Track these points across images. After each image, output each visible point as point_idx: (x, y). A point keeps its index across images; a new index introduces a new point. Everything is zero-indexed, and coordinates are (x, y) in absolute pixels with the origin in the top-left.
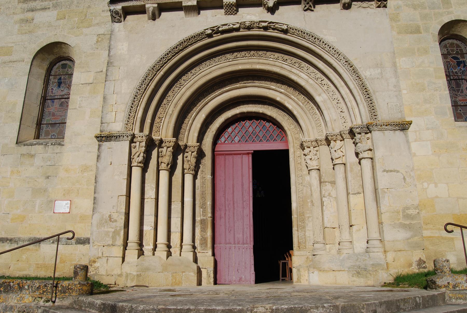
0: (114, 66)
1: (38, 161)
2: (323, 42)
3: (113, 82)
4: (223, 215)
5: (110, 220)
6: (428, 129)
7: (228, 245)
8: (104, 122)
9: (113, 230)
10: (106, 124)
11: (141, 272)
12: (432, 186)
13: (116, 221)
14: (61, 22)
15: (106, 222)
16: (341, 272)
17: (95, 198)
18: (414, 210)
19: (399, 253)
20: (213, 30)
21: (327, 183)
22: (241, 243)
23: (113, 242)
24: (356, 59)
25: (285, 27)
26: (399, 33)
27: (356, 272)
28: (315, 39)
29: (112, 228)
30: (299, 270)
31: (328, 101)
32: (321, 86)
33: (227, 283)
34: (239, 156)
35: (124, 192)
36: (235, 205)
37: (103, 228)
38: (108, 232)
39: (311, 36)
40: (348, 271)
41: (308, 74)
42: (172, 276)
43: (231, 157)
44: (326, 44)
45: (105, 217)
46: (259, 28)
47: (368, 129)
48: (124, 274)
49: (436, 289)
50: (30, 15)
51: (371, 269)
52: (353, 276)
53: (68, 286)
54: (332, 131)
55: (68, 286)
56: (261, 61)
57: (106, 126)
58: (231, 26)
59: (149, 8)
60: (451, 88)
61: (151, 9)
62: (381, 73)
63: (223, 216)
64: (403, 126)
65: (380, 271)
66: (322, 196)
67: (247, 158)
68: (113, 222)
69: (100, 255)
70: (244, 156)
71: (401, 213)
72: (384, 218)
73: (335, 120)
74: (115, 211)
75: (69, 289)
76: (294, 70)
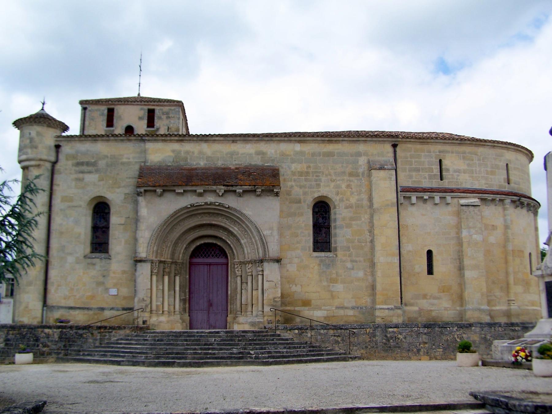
1: (98, 267)
6: (296, 258)
12: (294, 286)
14: (101, 183)
25: (227, 206)
28: (242, 214)
35: (149, 287)
50: (81, 176)
56: (215, 219)
60: (314, 232)
61: (159, 193)
64: (278, 261)
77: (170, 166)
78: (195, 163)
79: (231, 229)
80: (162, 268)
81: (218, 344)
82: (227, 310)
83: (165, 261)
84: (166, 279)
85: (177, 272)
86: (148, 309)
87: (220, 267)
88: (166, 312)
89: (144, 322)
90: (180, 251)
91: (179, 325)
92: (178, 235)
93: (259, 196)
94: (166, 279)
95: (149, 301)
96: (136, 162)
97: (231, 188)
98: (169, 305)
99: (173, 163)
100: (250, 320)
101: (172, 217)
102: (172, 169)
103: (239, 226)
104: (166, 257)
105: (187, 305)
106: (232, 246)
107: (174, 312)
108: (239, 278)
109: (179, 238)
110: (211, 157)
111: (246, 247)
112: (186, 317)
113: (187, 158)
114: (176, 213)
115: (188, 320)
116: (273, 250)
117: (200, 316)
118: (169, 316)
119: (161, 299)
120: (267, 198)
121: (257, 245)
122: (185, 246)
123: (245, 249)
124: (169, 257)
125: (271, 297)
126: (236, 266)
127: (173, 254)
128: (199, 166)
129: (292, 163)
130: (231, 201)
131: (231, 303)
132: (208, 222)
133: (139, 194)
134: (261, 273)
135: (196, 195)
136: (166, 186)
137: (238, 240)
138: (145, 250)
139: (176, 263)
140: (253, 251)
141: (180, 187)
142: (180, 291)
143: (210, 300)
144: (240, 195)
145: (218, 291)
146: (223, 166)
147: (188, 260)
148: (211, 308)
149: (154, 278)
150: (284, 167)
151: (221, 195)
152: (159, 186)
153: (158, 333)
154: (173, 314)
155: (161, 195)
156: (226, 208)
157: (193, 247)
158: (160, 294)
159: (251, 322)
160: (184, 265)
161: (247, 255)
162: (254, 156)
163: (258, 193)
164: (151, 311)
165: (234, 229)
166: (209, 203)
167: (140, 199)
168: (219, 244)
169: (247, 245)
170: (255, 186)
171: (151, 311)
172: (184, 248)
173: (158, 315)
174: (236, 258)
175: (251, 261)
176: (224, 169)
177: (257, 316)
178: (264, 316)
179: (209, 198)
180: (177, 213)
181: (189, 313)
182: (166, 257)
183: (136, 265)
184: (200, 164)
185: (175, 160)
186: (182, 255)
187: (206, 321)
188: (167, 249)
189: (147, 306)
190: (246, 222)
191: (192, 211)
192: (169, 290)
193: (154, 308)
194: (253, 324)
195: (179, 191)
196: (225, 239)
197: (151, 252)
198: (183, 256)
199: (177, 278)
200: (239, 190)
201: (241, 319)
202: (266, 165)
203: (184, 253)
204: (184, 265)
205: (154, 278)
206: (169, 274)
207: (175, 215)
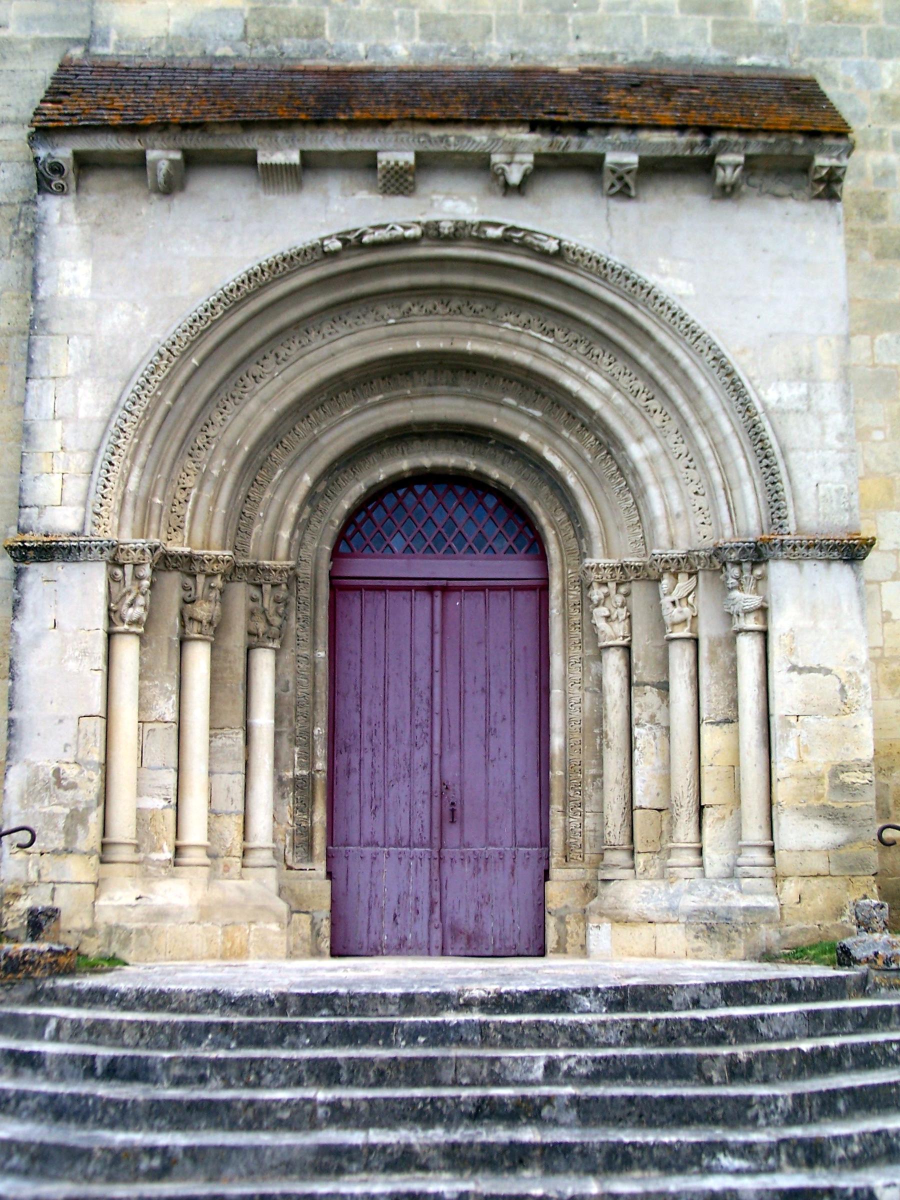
0: (50, 333)
2: (656, 298)
3: (51, 383)
4: (355, 765)
5: (58, 783)
7: (369, 849)
8: (27, 501)
9: (67, 811)
10: (35, 510)
11: (146, 924)
13: (73, 786)
15: (48, 789)
16: (668, 925)
17: (11, 723)
18: (861, 775)
19: (815, 881)
20: (345, 242)
21: (648, 688)
22: (405, 843)
23: (66, 842)
24: (743, 351)
25: (553, 246)
26: (880, 255)
27: (704, 927)
28: (637, 289)
29: (65, 806)
30: (562, 920)
31: (662, 461)
32: (647, 415)
33: (364, 951)
34: (404, 593)
35: (98, 707)
36: (392, 737)
37: (37, 806)
38: (53, 816)
39: (622, 278)
40: (687, 925)
41: (611, 379)
42: (225, 933)
43: (379, 596)
44: (662, 304)
45: (41, 775)
46: (479, 239)
47: (757, 554)
48: (102, 928)
49: (849, 965)
51: (741, 919)
52: (697, 937)
53: (24, 956)
54: (668, 546)
55: (24, 956)
56: (479, 328)
57: (35, 516)
58: (399, 231)
59: (155, 162)
61: (164, 166)
62: (808, 397)
63: (357, 767)
64: (852, 551)
65: (762, 926)
66: (634, 722)
67: (428, 600)
68: (66, 788)
69: (33, 876)
70: (418, 593)
71: (826, 781)
72: (781, 792)
73: (678, 516)
74: (72, 760)
75: (25, 963)
76: (572, 364)
77: (224, 58)
78: (361, 48)
79: (569, 383)
80: (172, 592)
81: (588, 1111)
82: (545, 842)
83: (190, 559)
84: (199, 657)
85: (261, 627)
86: (89, 838)
87: (499, 603)
88: (194, 856)
89: (39, 922)
90: (283, 508)
91: (274, 927)
92: (267, 417)
93: (727, 192)
94: (199, 657)
95: (90, 790)
96: (40, 44)
97: (572, 143)
98: (214, 813)
99: (244, 48)
100: (689, 902)
101: (238, 304)
102: (235, 71)
103: (619, 366)
104: (201, 534)
105: (320, 815)
106: (571, 480)
107: (245, 852)
108: (614, 661)
109: (274, 437)
110: (445, 18)
111: (660, 482)
112: (314, 881)
113: (319, 23)
114: (258, 280)
115: (328, 893)
116: (819, 496)
117: (393, 878)
118: (212, 877)
119: (170, 778)
120: (776, 208)
122: (308, 479)
123: (653, 492)
124: (217, 533)
125: (820, 760)
126: (597, 593)
127: (240, 521)
128: (387, 62)
129: (880, 55)
130: (568, 218)
131: (566, 800)
132: (441, 345)
133: (47, 179)
134: (751, 623)
135: (371, 189)
136: (200, 126)
137: (608, 444)
138: (76, 488)
139: (255, 574)
140: (701, 501)
141: (281, 135)
142: (277, 735)
143: (445, 787)
144: (623, 188)
145: (489, 732)
146: (511, 64)
147: (325, 565)
148: (452, 833)
149: (128, 651)
150: (840, 74)
151: (515, 176)
152: (163, 127)
153: (120, 1000)
154: (236, 862)
155: (170, 188)
157: (355, 489)
158: (162, 748)
159: (698, 912)
160: (305, 593)
161: (661, 527)
162: (677, 14)
163: (726, 176)
164: (105, 850)
165: (587, 383)
167: (53, 207)
168: (495, 474)
169: (666, 473)
170: (707, 131)
171: (105, 850)
173: (144, 870)
174: (598, 545)
175: (686, 558)
176: (524, 72)
177: (732, 875)
178: (778, 878)
179: (449, 205)
180: (262, 287)
181: (330, 857)
182: (199, 533)
183: (19, 573)
184: (388, 53)
185: (253, 30)
186: (287, 529)
187: (424, 906)
188: (207, 494)
189: (77, 818)
190: (662, 337)
191: (351, 277)
192: (215, 727)
193: (123, 827)
194: (714, 927)
195: (279, 158)
196: (536, 444)
197: (114, 505)
198: (297, 544)
199: (264, 661)
200: (621, 155)
201: (633, 892)
202: (744, 61)
203: (301, 525)
204: (305, 593)
205: (128, 651)
206: (216, 632)
207: (250, 296)
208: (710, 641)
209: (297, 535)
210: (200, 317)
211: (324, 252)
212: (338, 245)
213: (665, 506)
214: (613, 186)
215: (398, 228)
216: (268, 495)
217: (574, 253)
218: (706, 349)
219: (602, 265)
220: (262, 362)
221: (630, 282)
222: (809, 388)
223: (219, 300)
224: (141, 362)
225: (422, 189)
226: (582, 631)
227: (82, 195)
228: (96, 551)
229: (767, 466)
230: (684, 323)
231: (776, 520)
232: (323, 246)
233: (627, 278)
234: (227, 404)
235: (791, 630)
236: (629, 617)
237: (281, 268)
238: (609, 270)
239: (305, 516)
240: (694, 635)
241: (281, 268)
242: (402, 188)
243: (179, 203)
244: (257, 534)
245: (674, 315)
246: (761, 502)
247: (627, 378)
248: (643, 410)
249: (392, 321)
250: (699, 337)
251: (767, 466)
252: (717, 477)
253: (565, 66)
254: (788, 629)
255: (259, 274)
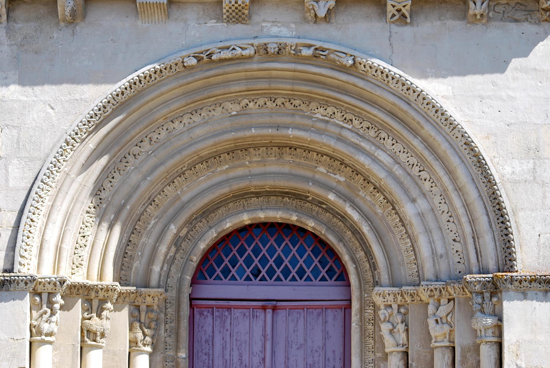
58: (239, 51)
73: (441, 256)
121: (472, 222)
140: (458, 246)
147: (187, 290)
151: (322, 13)
156: (343, 69)
166: (272, 48)
172: (169, 237)
204: (171, 311)
208: (462, 348)
209: (165, 268)
210: (95, 114)
211: (184, 66)
212: (194, 61)
213: (432, 250)
214: (394, 15)
215: (237, 48)
216: (143, 239)
217: (365, 66)
218: (460, 136)
219: (384, 75)
220: (139, 144)
221: (405, 88)
222: (535, 164)
223: (109, 102)
224: (54, 146)
225: (256, 18)
226: (375, 340)
227: (11, 23)
228: (22, 284)
229: (502, 222)
230: (443, 118)
231: (508, 262)
232: (183, 62)
233: (403, 85)
234: (115, 175)
235: (517, 341)
236: (407, 330)
237: (153, 79)
238: (390, 78)
239: (171, 254)
240: (452, 345)
241: (153, 79)
242: (240, 19)
243: (82, 28)
244: (136, 268)
245: (436, 112)
246: (498, 248)
247: (405, 155)
248: (417, 178)
249: (234, 113)
250: (454, 128)
251: (502, 222)
252: (467, 229)
253: (307, 55)
254: (515, 340)
255: (138, 83)
